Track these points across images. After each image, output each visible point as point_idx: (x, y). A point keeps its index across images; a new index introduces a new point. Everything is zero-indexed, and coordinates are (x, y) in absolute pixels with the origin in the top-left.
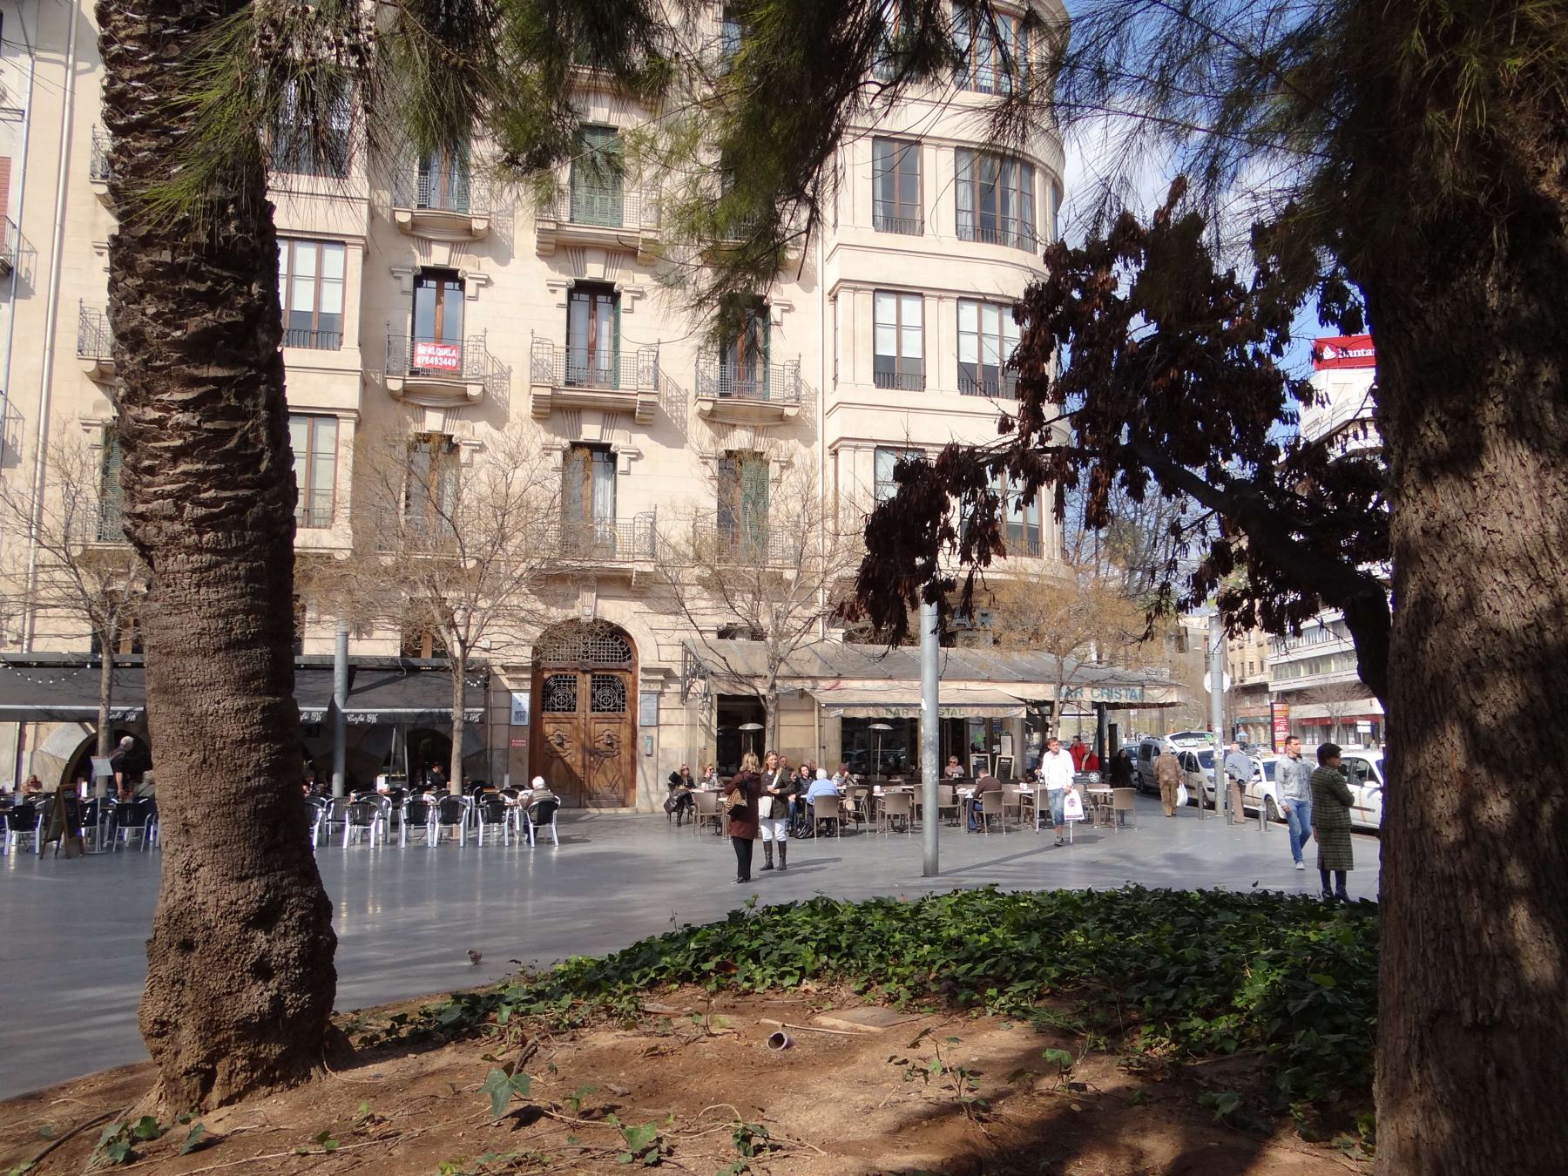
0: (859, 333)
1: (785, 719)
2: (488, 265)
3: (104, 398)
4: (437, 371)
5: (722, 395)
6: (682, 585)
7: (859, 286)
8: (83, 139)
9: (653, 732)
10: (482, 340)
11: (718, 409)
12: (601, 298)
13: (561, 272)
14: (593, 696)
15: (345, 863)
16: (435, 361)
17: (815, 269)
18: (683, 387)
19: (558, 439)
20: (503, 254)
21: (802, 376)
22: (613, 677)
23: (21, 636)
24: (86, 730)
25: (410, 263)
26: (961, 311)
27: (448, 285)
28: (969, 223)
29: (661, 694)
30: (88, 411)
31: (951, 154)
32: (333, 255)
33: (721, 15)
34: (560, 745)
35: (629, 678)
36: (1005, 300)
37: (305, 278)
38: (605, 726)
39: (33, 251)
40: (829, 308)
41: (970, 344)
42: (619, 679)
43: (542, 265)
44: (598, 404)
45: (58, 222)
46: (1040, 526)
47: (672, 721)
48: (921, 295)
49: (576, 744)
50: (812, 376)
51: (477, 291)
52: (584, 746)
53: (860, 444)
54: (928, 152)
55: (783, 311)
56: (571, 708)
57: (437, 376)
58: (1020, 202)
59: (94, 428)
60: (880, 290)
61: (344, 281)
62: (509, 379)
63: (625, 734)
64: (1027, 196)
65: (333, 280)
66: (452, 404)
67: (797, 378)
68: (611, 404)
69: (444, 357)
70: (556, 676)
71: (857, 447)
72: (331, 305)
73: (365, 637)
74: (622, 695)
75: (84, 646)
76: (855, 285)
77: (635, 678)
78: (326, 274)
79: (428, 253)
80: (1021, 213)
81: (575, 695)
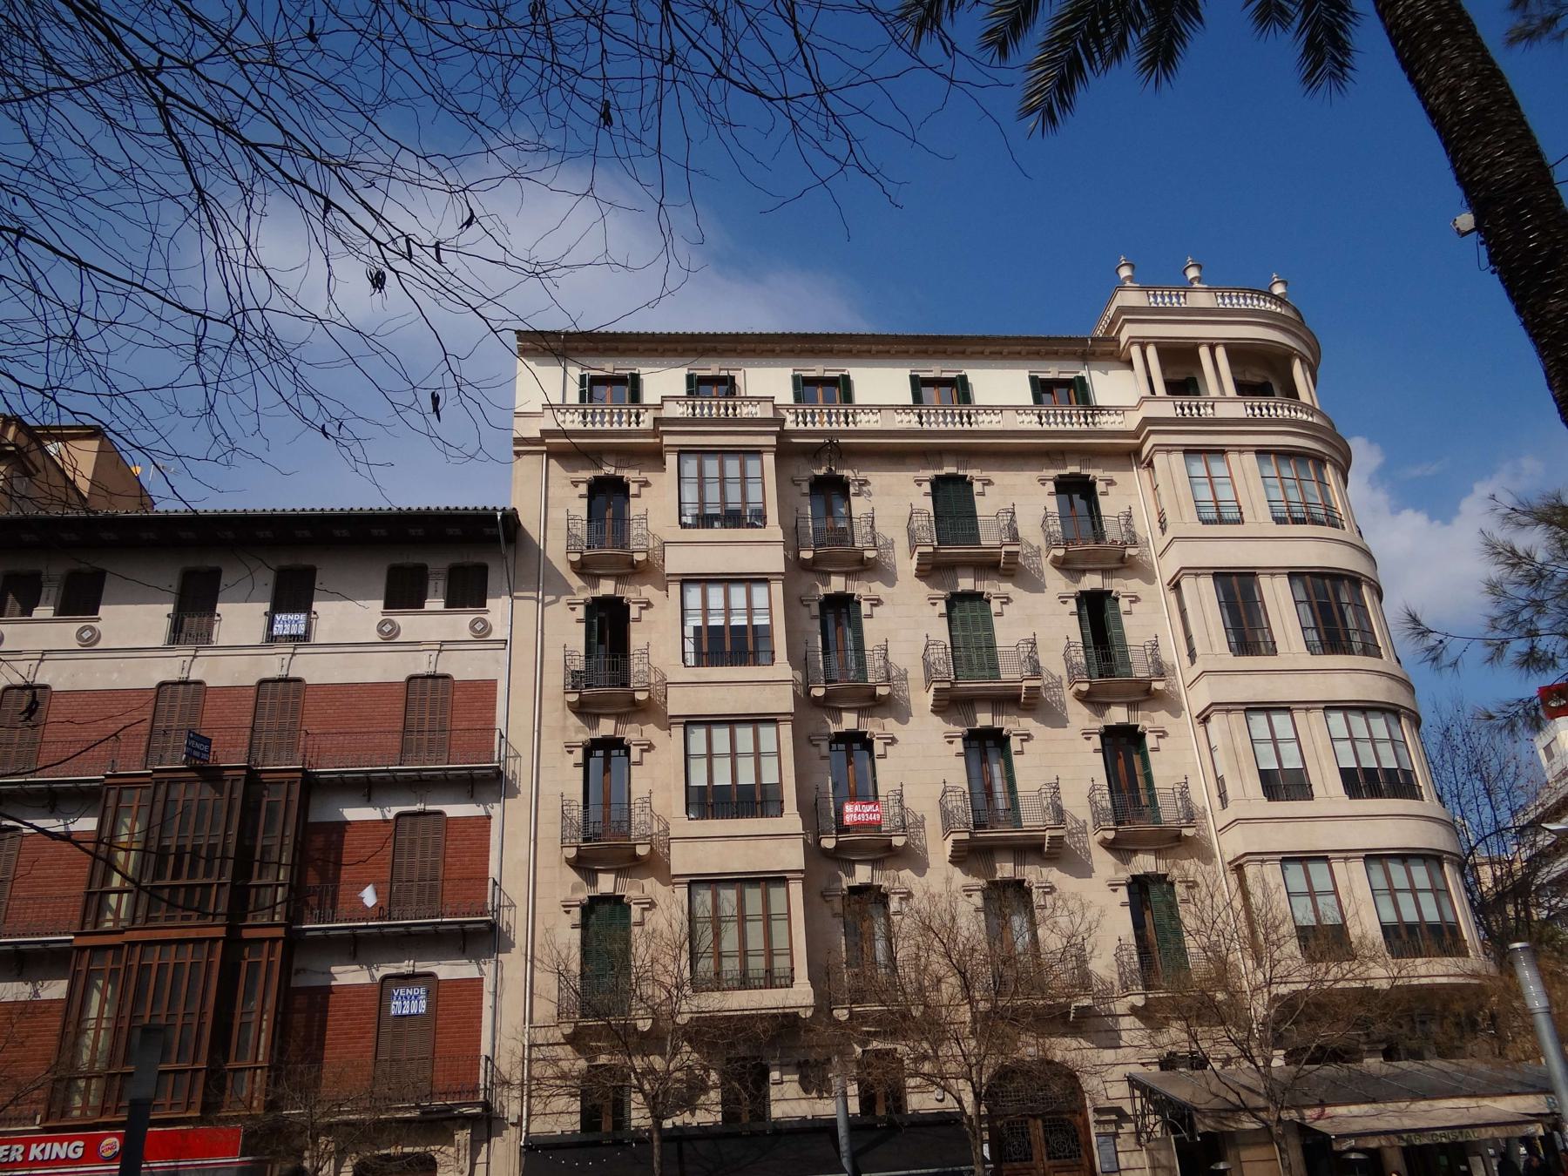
0: (1240, 750)
1: (1246, 1154)
2: (891, 725)
3: (580, 880)
4: (859, 826)
5: (585, 840)
6: (1116, 1016)
7: (1230, 707)
8: (554, 658)
10: (648, 800)
14: (1047, 1142)
16: (861, 818)
17: (1179, 695)
20: (903, 715)
21: (906, 804)
22: (1063, 1120)
25: (825, 731)
27: (615, 752)
28: (1316, 638)
29: (1116, 1135)
30: (567, 894)
31: (1210, 580)
32: (767, 732)
33: (1053, 489)
35: (1079, 1119)
37: (746, 755)
39: (518, 756)
41: (1266, 750)
42: (1070, 1122)
43: (937, 720)
44: (1011, 842)
45: (536, 728)
47: (1132, 1164)
50: (1202, 795)
51: (642, 757)
53: (1265, 857)
56: (1028, 1157)
57: (857, 832)
58: (1356, 615)
59: (572, 909)
60: (1251, 708)
61: (779, 754)
62: (923, 827)
64: (1360, 607)
65: (769, 754)
66: (879, 856)
67: (902, 808)
68: (1022, 842)
69: (869, 813)
71: (1263, 861)
72: (770, 777)
73: (825, 1095)
74: (1075, 1138)
76: (1227, 707)
78: (739, 750)
80: (1358, 621)
81: (1029, 1143)
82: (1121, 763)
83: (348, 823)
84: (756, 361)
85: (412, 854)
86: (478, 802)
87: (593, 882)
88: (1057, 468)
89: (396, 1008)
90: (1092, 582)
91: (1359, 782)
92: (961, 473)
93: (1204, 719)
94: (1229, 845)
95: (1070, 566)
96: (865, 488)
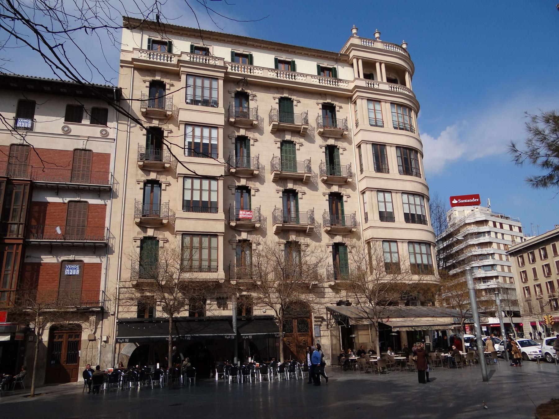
0: (374, 204)
1: (360, 333)
2: (258, 185)
3: (141, 230)
5: (143, 216)
7: (372, 189)
9: (319, 339)
10: (168, 204)
11: (142, 221)
12: (244, 191)
13: (280, 187)
14: (298, 327)
15: (269, 387)
18: (319, 222)
19: (283, 240)
20: (262, 182)
22: (304, 320)
23: (115, 313)
24: (136, 345)
26: (378, 195)
29: (321, 325)
30: (135, 235)
34: (289, 344)
35: (309, 320)
36: (421, 194)
38: (303, 337)
39: (118, 183)
40: (361, 196)
42: (306, 320)
43: (274, 184)
45: (126, 174)
46: (432, 265)
47: (325, 335)
48: (390, 192)
49: (294, 344)
52: (296, 344)
54: (388, 148)
55: (255, 191)
56: (292, 331)
63: (310, 339)
65: (214, 191)
66: (250, 230)
67: (260, 214)
69: (248, 215)
70: (286, 321)
72: (214, 199)
75: (134, 315)
76: (371, 189)
77: (311, 320)
78: (194, 188)
79: (239, 181)
80: (416, 166)
81: (292, 327)
82: (334, 205)
83: (49, 203)
84: (218, 43)
85: (75, 217)
86: (101, 199)
87: (145, 232)
88: (280, 94)
89: (67, 272)
90: (331, 142)
91: (410, 218)
92: (290, 97)
93: (363, 193)
94: (367, 235)
95: (324, 135)
96: (255, 98)
